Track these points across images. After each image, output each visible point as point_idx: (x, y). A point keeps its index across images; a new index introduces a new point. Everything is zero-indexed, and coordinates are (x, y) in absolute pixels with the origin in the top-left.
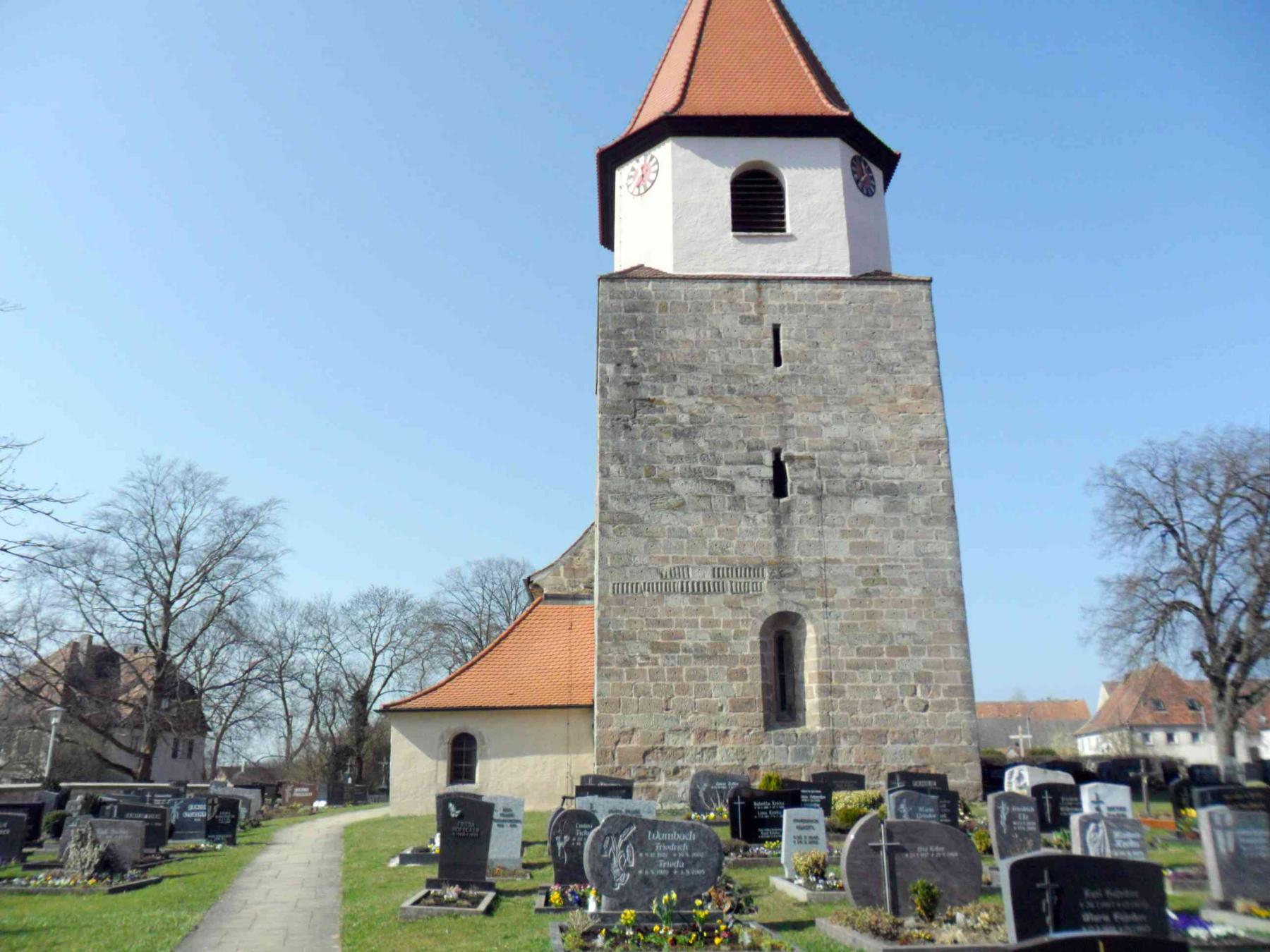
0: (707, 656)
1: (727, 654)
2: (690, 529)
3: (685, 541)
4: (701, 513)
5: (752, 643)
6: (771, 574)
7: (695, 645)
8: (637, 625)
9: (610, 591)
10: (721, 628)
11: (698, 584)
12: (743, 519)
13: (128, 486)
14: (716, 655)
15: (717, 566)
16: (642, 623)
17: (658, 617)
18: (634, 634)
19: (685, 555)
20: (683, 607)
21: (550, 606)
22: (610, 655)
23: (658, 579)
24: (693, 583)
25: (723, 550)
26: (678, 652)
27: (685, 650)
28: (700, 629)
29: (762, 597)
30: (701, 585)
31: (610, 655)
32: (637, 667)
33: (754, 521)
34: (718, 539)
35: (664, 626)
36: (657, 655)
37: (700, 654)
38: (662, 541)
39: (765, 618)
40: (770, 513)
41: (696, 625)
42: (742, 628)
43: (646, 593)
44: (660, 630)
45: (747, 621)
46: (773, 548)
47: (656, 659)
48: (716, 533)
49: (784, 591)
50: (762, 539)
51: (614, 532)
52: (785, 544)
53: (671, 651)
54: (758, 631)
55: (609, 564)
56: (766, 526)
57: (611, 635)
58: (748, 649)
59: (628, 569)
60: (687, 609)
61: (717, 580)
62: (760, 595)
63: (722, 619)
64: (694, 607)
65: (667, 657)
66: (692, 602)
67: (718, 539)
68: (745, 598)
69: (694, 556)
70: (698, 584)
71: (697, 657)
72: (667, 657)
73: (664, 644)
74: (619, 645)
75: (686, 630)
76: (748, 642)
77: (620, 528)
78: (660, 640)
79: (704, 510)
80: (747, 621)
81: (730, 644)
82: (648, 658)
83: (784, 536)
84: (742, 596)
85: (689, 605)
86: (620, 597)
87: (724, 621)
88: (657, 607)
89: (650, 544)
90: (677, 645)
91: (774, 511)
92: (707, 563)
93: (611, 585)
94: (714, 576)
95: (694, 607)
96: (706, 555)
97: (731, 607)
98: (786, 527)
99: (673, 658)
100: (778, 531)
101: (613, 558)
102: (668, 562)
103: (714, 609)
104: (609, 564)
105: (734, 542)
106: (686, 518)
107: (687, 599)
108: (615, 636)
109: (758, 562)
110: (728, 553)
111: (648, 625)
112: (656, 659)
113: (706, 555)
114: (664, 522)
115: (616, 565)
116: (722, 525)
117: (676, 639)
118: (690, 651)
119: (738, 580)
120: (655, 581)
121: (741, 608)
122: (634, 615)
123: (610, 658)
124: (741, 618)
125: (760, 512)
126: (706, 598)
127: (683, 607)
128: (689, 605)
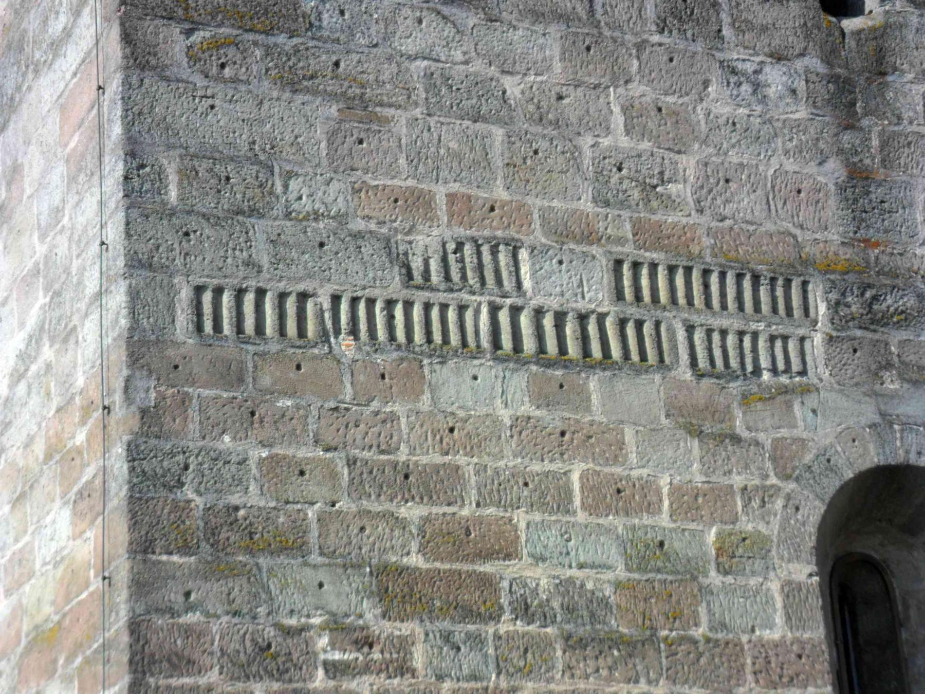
0: (616, 641)
1: (699, 632)
2: (513, 87)
3: (499, 133)
4: (555, 30)
5: (791, 589)
6: (835, 306)
7: (564, 586)
8: (312, 487)
9: (183, 319)
10: (664, 520)
11: (560, 319)
12: (716, 76)
13: (426, 262)
14: (652, 639)
15: (628, 250)
16: (334, 476)
17: (403, 455)
18: (299, 526)
19: (501, 193)
20: (505, 415)
21: (605, 281)
22: (192, 618)
23: (394, 286)
24: (539, 313)
25: (649, 189)
26: (495, 617)
27: (524, 610)
28: (581, 517)
29: (812, 401)
30: (570, 329)
31: (192, 618)
32: (320, 679)
33: (757, 87)
34: (624, 142)
35: (428, 495)
36: (406, 628)
37: (584, 631)
38: (400, 122)
39: (832, 485)
40: (814, 62)
41: (563, 504)
42: (747, 525)
43: (345, 345)
44: (412, 512)
45: (766, 494)
46: (832, 207)
47: (404, 645)
48: (618, 120)
49: (891, 384)
50: (790, 165)
51: (192, 56)
52: (877, 193)
53: (468, 613)
54: (811, 542)
55: (173, 194)
56: (802, 113)
57: (195, 522)
58: (779, 619)
59: (261, 229)
60: (520, 423)
61: (633, 311)
62: (806, 390)
63: (664, 482)
64: (552, 419)
65: (447, 637)
66: (542, 399)
67: (624, 142)
68: (745, 399)
69: (535, 203)
70: (560, 319)
71: (572, 643)
72: (447, 637)
73: (432, 577)
74: (233, 572)
75: (521, 518)
76: (774, 586)
77: (217, 44)
78: (415, 560)
79: (565, 18)
80: (766, 494)
81: (706, 591)
82: (366, 642)
83: (871, 160)
84: (735, 387)
85: (527, 409)
86: (230, 349)
87: (676, 491)
88: (397, 407)
89: (356, 128)
90: (487, 583)
91: (828, 62)
92: (590, 237)
93: (185, 294)
94: (619, 296)
95: (552, 419)
96: (586, 205)
97: (699, 434)
98: (874, 128)
99: (477, 641)
100: (847, 138)
101: (188, 175)
102: (430, 216)
103: (629, 435)
104: (173, 194)
105: (689, 164)
106: (495, 39)
107: (518, 381)
108: (212, 532)
109: (783, 252)
110: (669, 203)
111: (356, 488)
112: (404, 645)
113: (586, 205)
114: (409, 46)
115: (207, 204)
116: (637, 89)
117: (487, 555)
118: (547, 619)
119: (718, 322)
120: (380, 295)
121: (736, 439)
122: (293, 437)
123: (188, 631)
124: (738, 480)
125: (778, 57)
126: (594, 383)
127: (505, 415)
128: (527, 409)
